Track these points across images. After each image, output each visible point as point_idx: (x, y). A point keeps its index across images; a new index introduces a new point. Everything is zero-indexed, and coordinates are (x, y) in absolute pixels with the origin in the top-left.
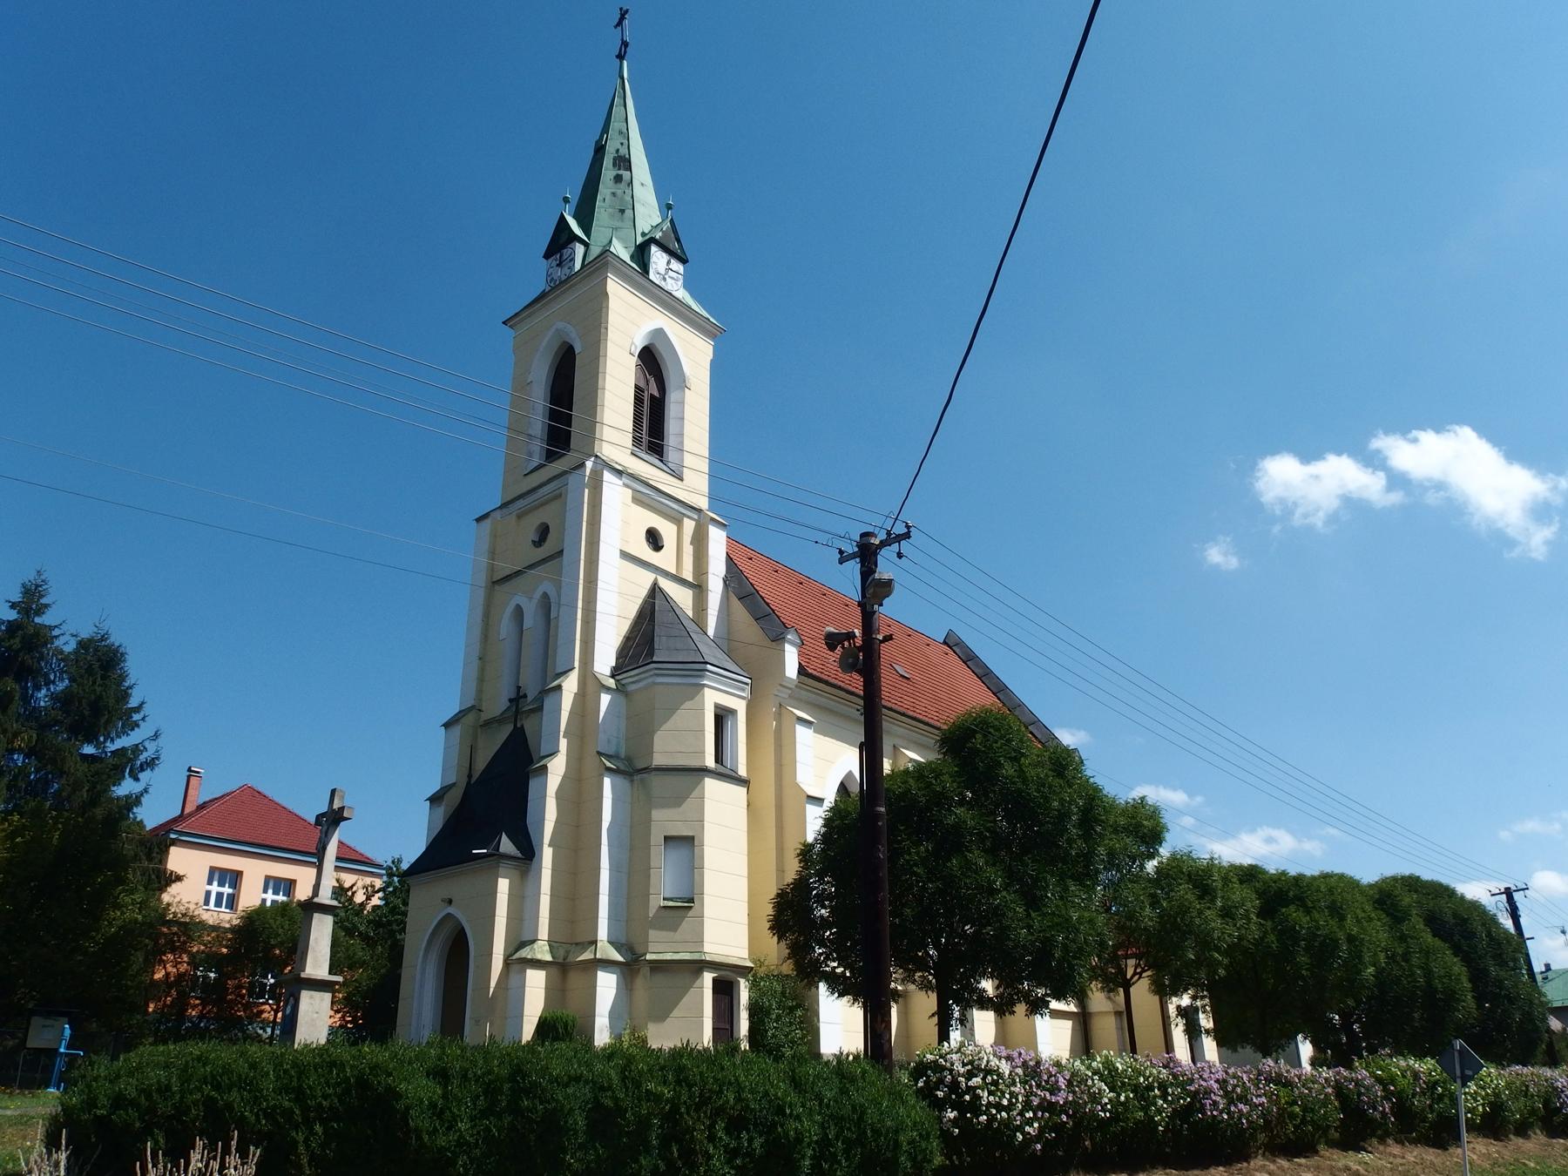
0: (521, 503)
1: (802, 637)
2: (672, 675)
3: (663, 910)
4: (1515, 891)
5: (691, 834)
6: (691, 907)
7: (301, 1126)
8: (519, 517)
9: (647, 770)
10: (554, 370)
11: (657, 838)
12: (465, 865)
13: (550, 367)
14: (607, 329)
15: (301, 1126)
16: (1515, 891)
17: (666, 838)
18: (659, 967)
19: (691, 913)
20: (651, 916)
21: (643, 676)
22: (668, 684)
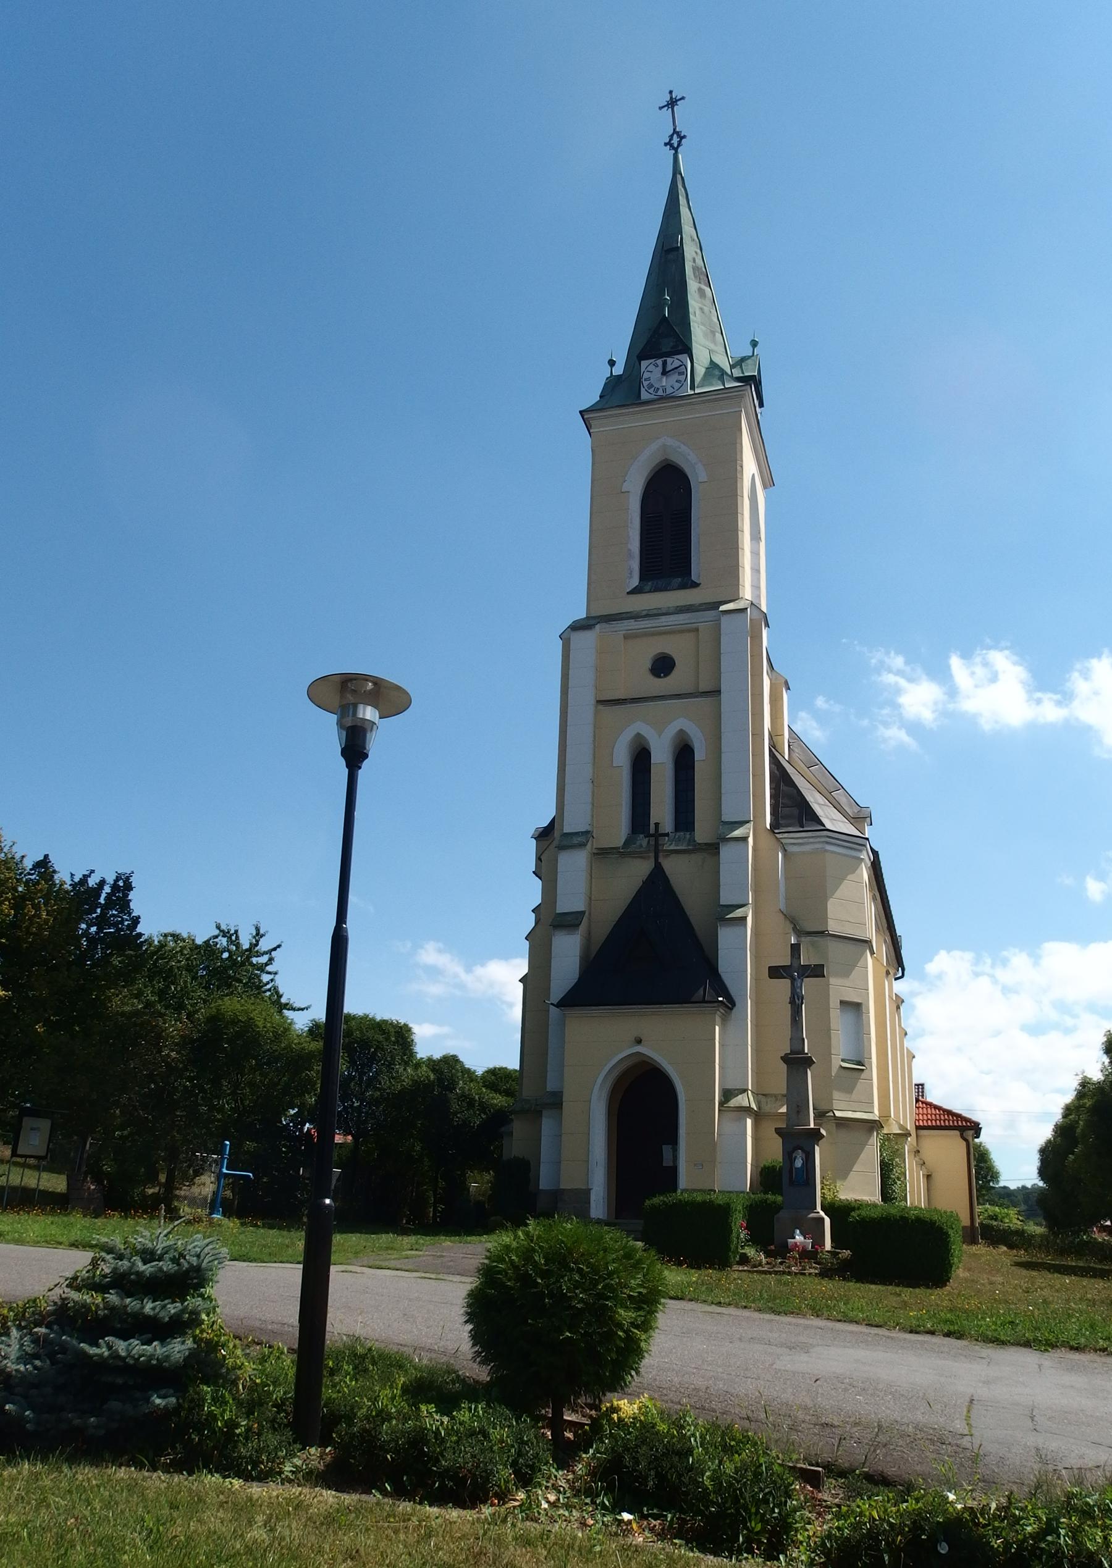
0: (632, 624)
1: (783, 841)
2: (839, 845)
3: (842, 1070)
4: (665, 363)
5: (860, 1001)
6: (863, 1070)
7: (749, 1092)
8: (626, 637)
9: (822, 933)
10: (654, 472)
11: (834, 1003)
12: (665, 1006)
13: (651, 471)
14: (742, 467)
15: (749, 1092)
16: (665, 363)
17: (842, 1002)
18: (843, 1123)
19: (863, 1075)
20: (833, 1075)
21: (811, 840)
22: (835, 853)
